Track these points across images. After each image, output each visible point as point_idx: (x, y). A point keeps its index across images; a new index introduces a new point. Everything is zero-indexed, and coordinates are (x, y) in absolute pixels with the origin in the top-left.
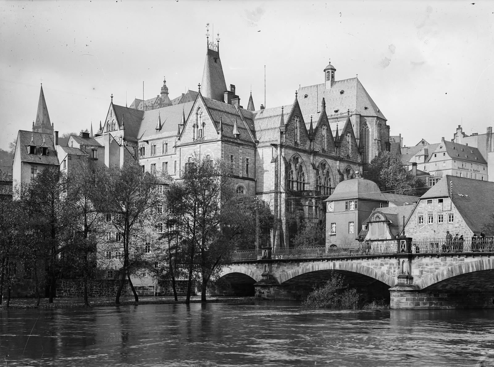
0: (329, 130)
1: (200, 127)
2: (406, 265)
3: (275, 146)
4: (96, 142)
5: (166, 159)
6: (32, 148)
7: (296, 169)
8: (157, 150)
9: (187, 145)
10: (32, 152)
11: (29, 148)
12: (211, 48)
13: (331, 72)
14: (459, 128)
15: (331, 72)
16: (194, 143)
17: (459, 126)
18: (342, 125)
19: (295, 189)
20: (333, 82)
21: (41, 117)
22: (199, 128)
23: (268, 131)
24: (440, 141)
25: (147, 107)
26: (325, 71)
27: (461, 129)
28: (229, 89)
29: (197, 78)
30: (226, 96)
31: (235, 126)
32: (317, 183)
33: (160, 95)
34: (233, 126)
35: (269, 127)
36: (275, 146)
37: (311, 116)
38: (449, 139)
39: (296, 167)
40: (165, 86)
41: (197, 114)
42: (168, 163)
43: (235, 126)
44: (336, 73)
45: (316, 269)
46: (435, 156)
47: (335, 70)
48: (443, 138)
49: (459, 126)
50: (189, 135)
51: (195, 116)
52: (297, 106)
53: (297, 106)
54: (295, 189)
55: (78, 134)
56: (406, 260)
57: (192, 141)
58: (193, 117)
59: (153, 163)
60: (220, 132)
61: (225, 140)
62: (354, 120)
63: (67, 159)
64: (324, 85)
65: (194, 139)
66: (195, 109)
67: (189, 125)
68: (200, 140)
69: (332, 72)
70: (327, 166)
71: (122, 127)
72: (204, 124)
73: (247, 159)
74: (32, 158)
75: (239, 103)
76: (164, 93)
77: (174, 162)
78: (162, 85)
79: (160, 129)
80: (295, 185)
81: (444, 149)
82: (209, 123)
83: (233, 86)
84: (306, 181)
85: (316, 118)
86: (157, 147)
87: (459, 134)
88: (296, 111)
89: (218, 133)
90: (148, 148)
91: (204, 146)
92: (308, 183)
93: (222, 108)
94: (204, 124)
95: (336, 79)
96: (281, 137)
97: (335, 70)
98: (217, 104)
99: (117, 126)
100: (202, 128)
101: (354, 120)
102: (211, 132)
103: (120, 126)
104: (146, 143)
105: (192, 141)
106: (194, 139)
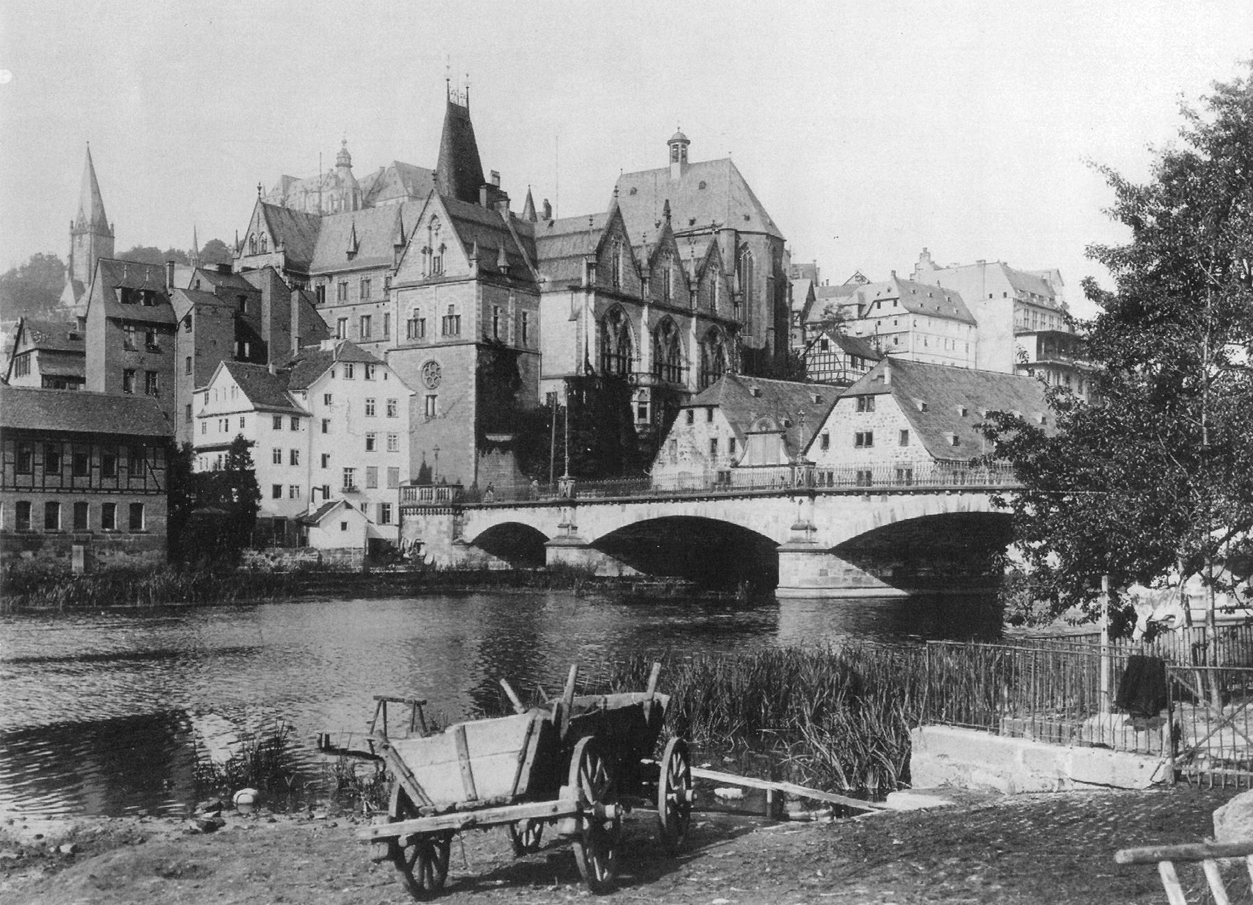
1: (436, 253)
5: (369, 310)
6: (126, 292)
7: (616, 334)
8: (350, 293)
10: (125, 300)
11: (119, 291)
12: (453, 99)
13: (679, 147)
14: (926, 253)
15: (679, 147)
18: (701, 250)
19: (614, 370)
20: (686, 166)
23: (562, 256)
24: (888, 278)
25: (307, 192)
26: (669, 143)
27: (929, 255)
28: (488, 179)
29: (427, 151)
30: (483, 193)
31: (502, 251)
32: (603, 349)
33: (335, 169)
34: (497, 251)
35: (564, 254)
37: (642, 230)
38: (904, 275)
39: (615, 328)
40: (345, 152)
42: (373, 318)
43: (502, 251)
44: (689, 147)
45: (691, 513)
46: (879, 307)
47: (688, 142)
48: (894, 272)
50: (416, 267)
52: (617, 214)
53: (617, 214)
54: (614, 370)
55: (122, 246)
57: (421, 278)
58: (423, 234)
59: (342, 316)
60: (474, 262)
61: (487, 276)
62: (725, 240)
63: (193, 313)
64: (668, 171)
66: (427, 218)
67: (414, 249)
68: (437, 278)
69: (683, 146)
70: (673, 327)
71: (280, 248)
72: (443, 248)
73: (525, 314)
74: (130, 312)
75: (508, 206)
76: (344, 165)
77: (383, 316)
78: (339, 148)
80: (614, 362)
82: (455, 245)
83: (495, 175)
85: (654, 238)
86: (350, 285)
87: (925, 265)
89: (471, 266)
90: (332, 288)
91: (444, 289)
93: (476, 217)
94: (443, 248)
95: (692, 159)
97: (688, 142)
98: (466, 209)
99: (270, 247)
100: (439, 254)
101: (725, 240)
102: (458, 262)
103: (276, 244)
104: (327, 279)
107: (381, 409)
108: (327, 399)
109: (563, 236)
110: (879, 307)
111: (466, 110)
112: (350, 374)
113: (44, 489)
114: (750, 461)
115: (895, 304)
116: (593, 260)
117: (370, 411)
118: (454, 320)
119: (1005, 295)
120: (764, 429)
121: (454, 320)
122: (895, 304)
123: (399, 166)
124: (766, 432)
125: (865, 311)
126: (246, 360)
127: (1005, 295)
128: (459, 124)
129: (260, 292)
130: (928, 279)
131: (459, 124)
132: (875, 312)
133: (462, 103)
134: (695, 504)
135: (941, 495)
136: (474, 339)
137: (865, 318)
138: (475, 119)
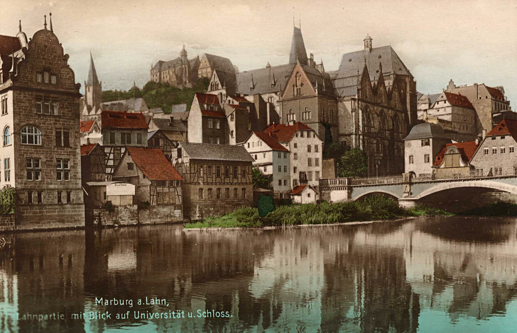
0: (385, 87)
2: (408, 187)
3: (354, 100)
4: (246, 100)
9: (289, 100)
12: (296, 26)
16: (295, 99)
17: (451, 80)
21: (92, 78)
22: (298, 87)
26: (364, 40)
36: (354, 100)
41: (296, 77)
44: (372, 41)
45: (472, 185)
46: (438, 104)
49: (451, 80)
51: (294, 78)
56: (408, 185)
63: (234, 113)
65: (294, 95)
70: (383, 114)
71: (224, 87)
79: (253, 88)
81: (445, 98)
84: (372, 126)
88: (366, 74)
92: (374, 127)
94: (302, 85)
96: (358, 93)
103: (222, 86)
105: (293, 97)
106: (294, 95)
107: (313, 149)
108: (295, 146)
109: (342, 78)
110: (438, 104)
111: (300, 30)
112: (302, 136)
113: (216, 184)
114: (445, 166)
115: (445, 103)
116: (360, 87)
117: (309, 150)
118: (307, 113)
119: (487, 97)
120: (452, 152)
121: (307, 113)
122: (445, 103)
123: (210, 58)
124: (453, 154)
125: (431, 107)
126: (492, 115)
127: (487, 97)
128: (298, 34)
129: (253, 104)
130: (456, 92)
131: (298, 34)
132: (436, 106)
133: (298, 27)
134: (449, 183)
135: (460, 182)
136: (317, 121)
137: (432, 108)
138: (302, 32)
